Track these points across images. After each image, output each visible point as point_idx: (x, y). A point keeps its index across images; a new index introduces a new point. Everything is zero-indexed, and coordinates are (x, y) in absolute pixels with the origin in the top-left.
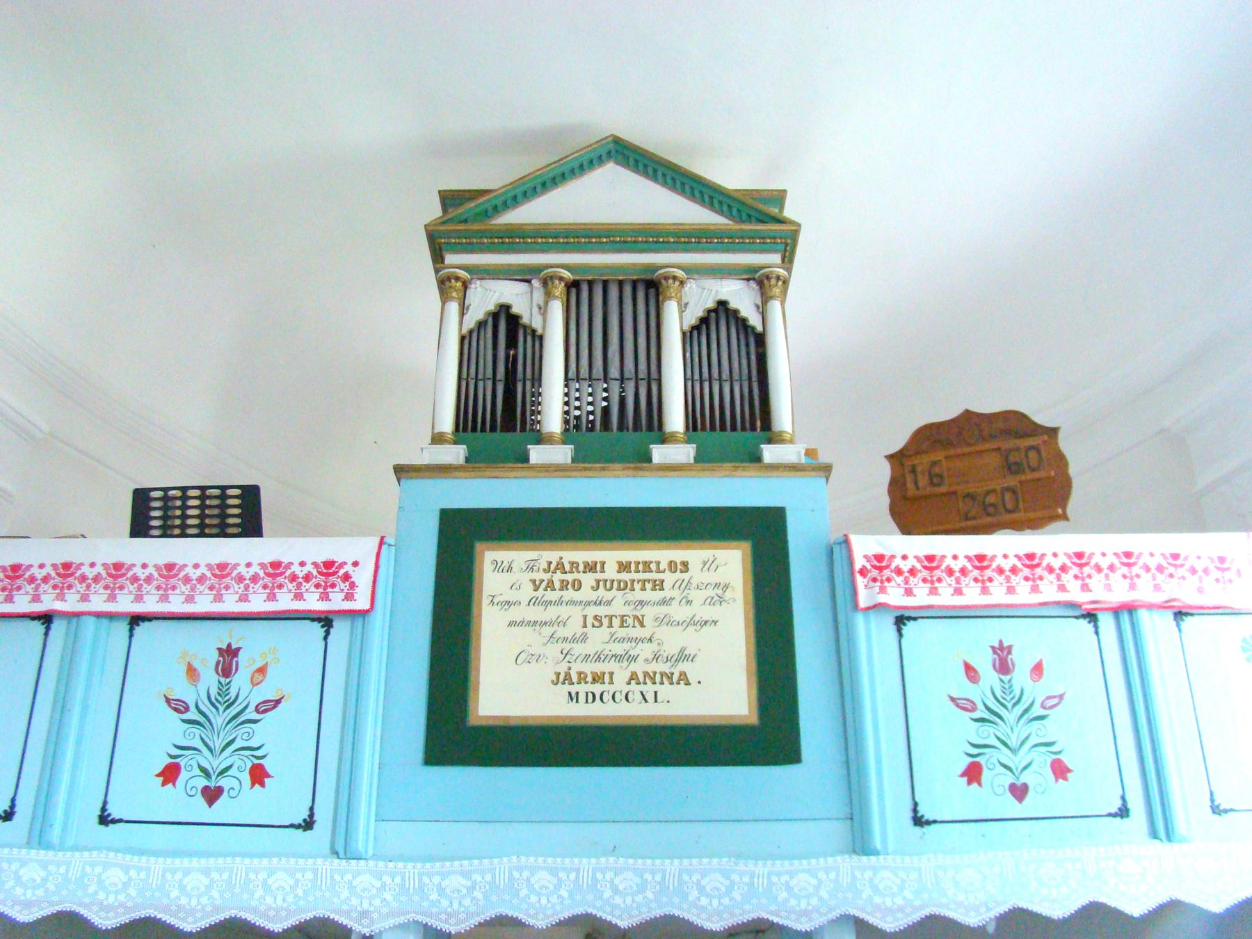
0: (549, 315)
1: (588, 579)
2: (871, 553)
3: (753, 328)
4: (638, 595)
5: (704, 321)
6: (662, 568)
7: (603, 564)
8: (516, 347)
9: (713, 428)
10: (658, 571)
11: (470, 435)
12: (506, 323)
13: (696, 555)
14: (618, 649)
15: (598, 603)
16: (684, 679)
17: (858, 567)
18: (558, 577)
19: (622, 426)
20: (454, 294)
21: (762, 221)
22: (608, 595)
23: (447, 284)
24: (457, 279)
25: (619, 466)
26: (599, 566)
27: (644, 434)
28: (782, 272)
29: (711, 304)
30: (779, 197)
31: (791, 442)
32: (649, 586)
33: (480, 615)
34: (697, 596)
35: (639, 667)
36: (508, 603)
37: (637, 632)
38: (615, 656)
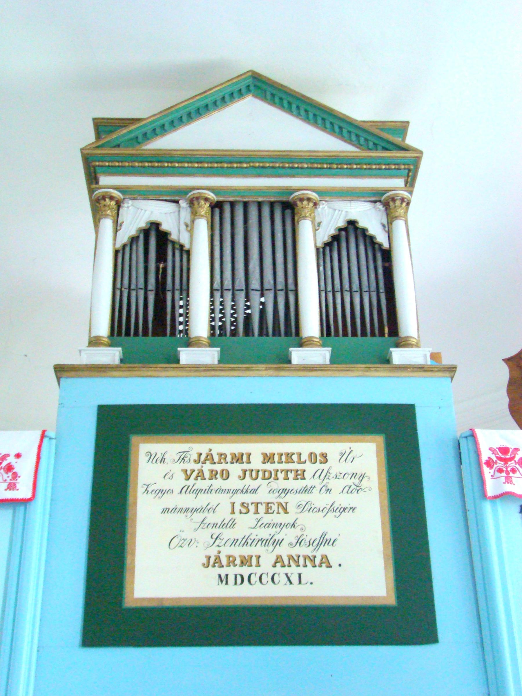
0: (196, 231)
1: (236, 469)
2: (496, 446)
3: (380, 245)
4: (282, 484)
5: (336, 238)
6: (303, 459)
7: (249, 455)
8: (165, 261)
9: (345, 334)
10: (300, 462)
11: (123, 338)
12: (156, 237)
13: (333, 447)
14: (264, 533)
15: (245, 491)
16: (326, 562)
17: (484, 458)
18: (207, 467)
19: (263, 332)
20: (108, 212)
21: (385, 149)
22: (254, 484)
23: (102, 202)
24: (112, 198)
25: (262, 366)
26: (245, 458)
27: (283, 339)
28: (406, 194)
29: (342, 224)
30: (402, 128)
31: (417, 346)
32: (291, 475)
33: (135, 504)
34: (336, 485)
35: (284, 551)
36: (161, 491)
37: (282, 518)
38: (261, 540)
